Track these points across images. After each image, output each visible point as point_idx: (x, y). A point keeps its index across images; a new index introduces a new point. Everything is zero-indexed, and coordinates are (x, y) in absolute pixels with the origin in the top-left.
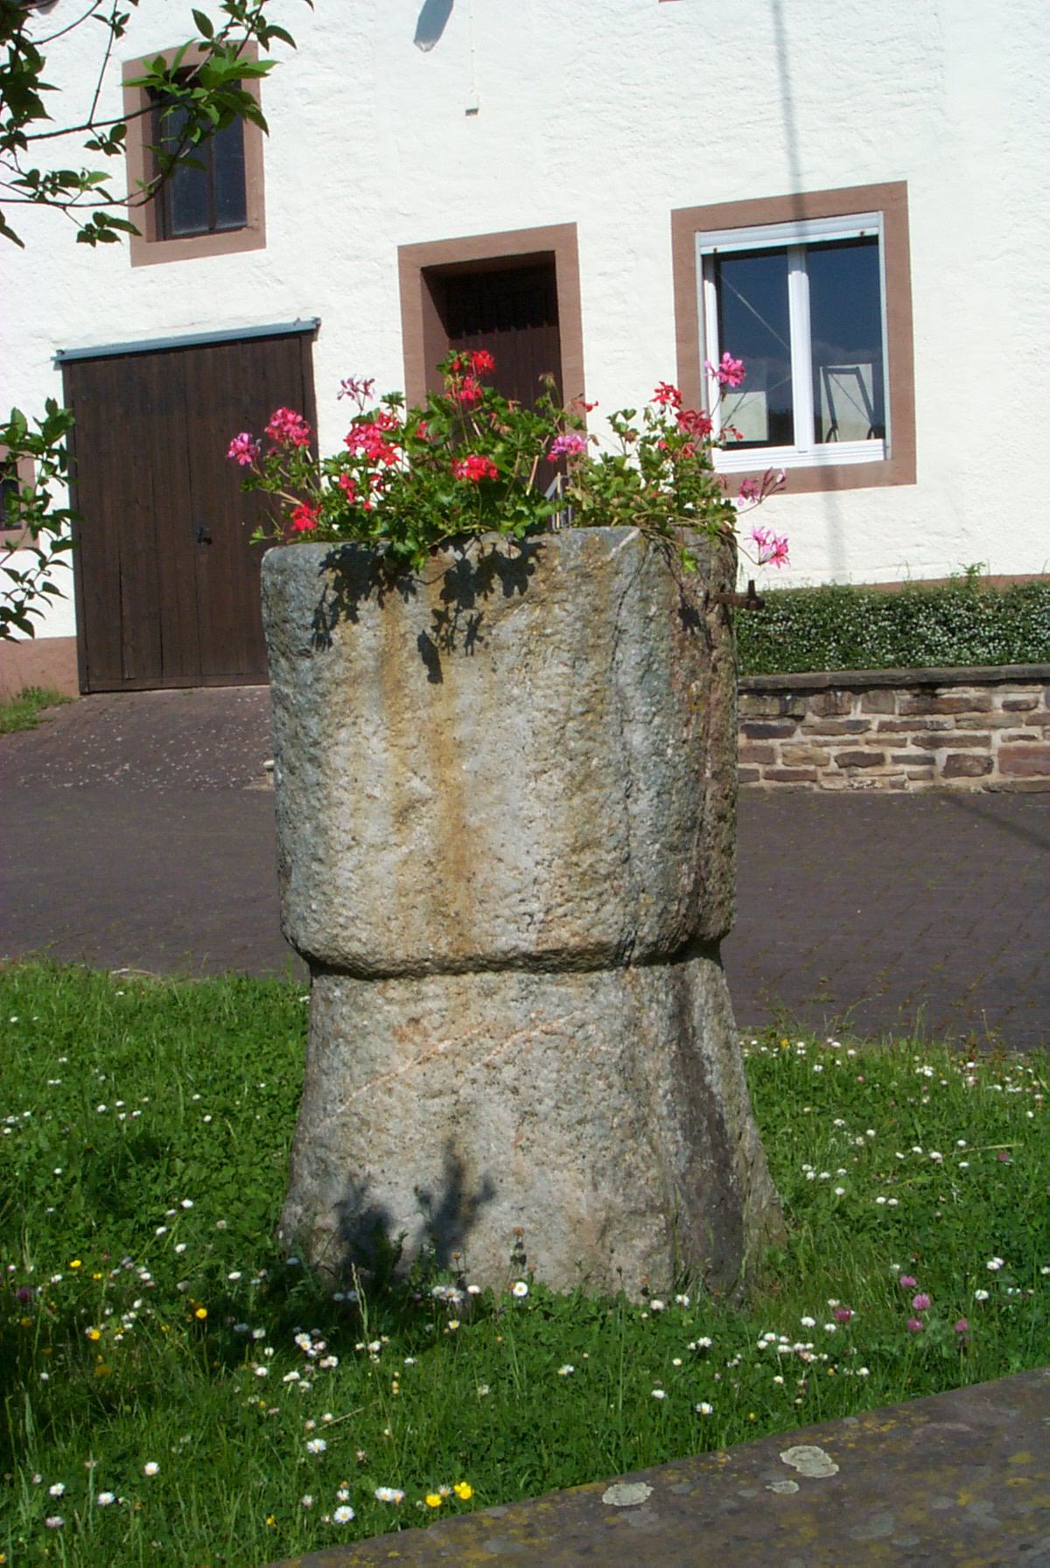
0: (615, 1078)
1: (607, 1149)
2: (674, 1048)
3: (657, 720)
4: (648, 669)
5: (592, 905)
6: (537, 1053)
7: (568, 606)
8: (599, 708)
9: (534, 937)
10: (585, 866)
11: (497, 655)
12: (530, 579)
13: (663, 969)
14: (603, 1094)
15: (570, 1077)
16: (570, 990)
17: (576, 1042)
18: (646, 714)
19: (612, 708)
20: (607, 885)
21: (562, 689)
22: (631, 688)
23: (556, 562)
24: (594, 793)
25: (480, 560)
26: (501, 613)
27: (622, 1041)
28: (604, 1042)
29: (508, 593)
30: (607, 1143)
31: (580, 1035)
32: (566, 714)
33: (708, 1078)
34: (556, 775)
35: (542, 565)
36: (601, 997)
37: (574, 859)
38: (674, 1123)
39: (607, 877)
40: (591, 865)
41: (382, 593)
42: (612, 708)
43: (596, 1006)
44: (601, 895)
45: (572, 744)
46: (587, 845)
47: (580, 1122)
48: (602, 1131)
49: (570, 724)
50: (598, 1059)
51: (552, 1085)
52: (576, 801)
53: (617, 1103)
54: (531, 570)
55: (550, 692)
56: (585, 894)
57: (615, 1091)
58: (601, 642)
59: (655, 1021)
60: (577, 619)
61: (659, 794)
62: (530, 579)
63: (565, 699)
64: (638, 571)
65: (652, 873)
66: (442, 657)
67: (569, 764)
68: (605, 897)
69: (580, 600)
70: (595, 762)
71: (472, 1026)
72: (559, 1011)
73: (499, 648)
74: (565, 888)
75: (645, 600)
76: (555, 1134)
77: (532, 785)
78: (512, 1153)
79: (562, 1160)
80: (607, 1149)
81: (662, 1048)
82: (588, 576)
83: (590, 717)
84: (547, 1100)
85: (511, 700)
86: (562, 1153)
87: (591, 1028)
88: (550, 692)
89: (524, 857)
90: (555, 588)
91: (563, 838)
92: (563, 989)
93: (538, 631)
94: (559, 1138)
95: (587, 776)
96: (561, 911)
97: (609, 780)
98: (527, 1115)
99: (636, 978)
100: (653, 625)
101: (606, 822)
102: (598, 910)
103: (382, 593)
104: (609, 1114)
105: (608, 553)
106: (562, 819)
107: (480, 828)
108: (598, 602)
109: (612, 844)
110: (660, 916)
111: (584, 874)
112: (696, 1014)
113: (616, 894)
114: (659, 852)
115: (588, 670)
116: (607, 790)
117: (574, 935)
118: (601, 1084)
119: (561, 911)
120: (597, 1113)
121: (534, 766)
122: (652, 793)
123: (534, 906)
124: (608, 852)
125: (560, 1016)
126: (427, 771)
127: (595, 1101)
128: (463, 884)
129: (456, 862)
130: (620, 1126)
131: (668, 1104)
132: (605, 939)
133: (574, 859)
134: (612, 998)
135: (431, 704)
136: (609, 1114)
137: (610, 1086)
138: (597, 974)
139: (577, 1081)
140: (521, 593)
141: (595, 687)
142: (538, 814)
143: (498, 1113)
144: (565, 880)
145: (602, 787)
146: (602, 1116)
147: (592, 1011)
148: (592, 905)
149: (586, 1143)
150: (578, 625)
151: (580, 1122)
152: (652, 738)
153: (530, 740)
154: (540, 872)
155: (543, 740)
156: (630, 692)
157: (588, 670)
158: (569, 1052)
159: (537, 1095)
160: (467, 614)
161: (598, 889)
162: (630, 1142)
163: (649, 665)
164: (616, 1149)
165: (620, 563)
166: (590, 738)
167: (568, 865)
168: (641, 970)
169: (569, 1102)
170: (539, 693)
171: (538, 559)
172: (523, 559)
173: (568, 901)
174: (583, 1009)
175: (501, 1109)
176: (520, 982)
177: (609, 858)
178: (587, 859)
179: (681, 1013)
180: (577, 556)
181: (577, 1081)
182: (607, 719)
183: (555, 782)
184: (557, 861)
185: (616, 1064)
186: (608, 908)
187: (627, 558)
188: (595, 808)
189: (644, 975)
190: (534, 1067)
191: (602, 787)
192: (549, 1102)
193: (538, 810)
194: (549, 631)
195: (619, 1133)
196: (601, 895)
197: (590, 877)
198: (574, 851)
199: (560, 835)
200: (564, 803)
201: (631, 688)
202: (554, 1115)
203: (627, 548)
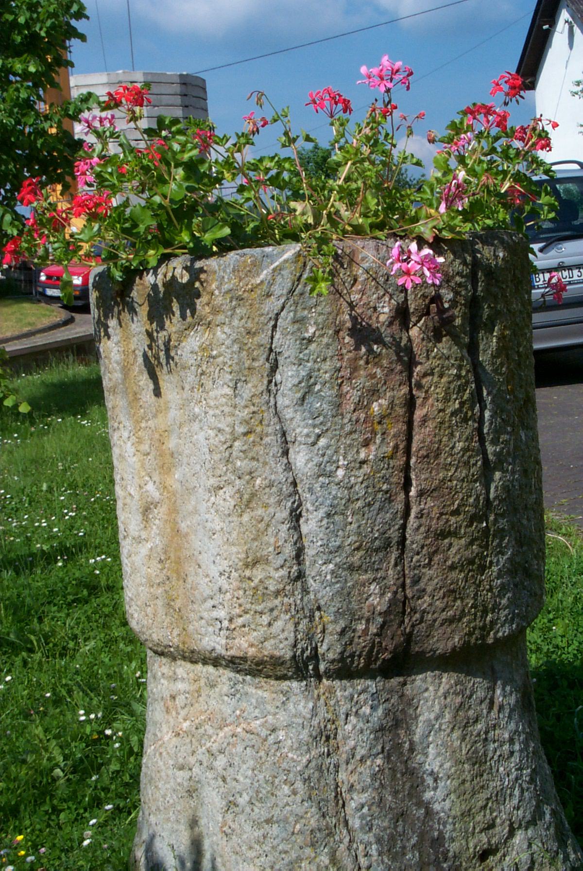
0: (299, 785)
1: (286, 852)
2: (379, 761)
3: (322, 442)
4: (309, 390)
5: (265, 619)
6: (240, 748)
7: (226, 329)
8: (259, 429)
9: (224, 641)
10: (256, 581)
11: (182, 373)
12: (198, 302)
13: (369, 682)
14: (290, 800)
15: (261, 777)
16: (266, 694)
17: (267, 744)
18: (307, 436)
19: (270, 430)
20: (277, 602)
21: (227, 409)
22: (290, 410)
23: (214, 286)
24: (260, 512)
25: (164, 285)
26: (183, 334)
27: (309, 751)
28: (291, 749)
29: (183, 317)
30: (287, 847)
31: (271, 739)
32: (232, 433)
33: (428, 795)
34: (229, 491)
35: (204, 288)
36: (291, 706)
37: (248, 573)
38: (370, 837)
39: (277, 593)
40: (261, 581)
41: (119, 313)
42: (270, 430)
43: (291, 708)
44: (272, 610)
45: (239, 463)
46: (255, 562)
47: (268, 821)
48: (284, 835)
49: (237, 444)
50: (284, 765)
51: (248, 781)
52: (246, 518)
53: (300, 810)
54: (199, 296)
55: (218, 412)
56: (259, 608)
57: (298, 798)
58: (256, 364)
59: (354, 735)
60: (234, 341)
61: (329, 515)
62: (198, 302)
63: (229, 419)
64: (291, 292)
65: (328, 592)
66: (157, 370)
67: (238, 482)
68: (275, 613)
69: (236, 323)
70: (258, 482)
71: (201, 713)
72: (257, 712)
73: (184, 368)
74: (241, 601)
75: (300, 321)
76: (247, 828)
77: (213, 498)
78: (220, 836)
79: (251, 854)
80: (286, 852)
81: (362, 760)
82: (240, 299)
83: (252, 438)
84: (245, 795)
85: (195, 417)
86: (251, 848)
87: (281, 735)
88: (218, 412)
89: (212, 566)
90: (216, 311)
91: (237, 553)
92: (260, 692)
93: (207, 353)
94: (251, 833)
95: (253, 495)
96: (240, 621)
97: (272, 500)
98: (231, 805)
99: (331, 691)
100: (313, 346)
101: (272, 540)
102: (270, 624)
103: (119, 313)
104: (292, 819)
105: (258, 275)
106: (234, 535)
107: (187, 534)
108: (249, 325)
109: (280, 562)
110: (343, 633)
111: (256, 588)
112: (419, 730)
113: (286, 612)
114: (333, 572)
115: (247, 391)
116: (271, 510)
117: (252, 645)
118: (286, 789)
119: (240, 621)
120: (281, 817)
121: (213, 481)
122: (321, 513)
123: (222, 613)
124: (277, 569)
125: (256, 718)
126: (156, 478)
127: (281, 804)
128: (181, 582)
129: (176, 563)
130: (301, 832)
131: (362, 817)
132: (277, 653)
133: (248, 573)
134: (300, 707)
135: (155, 416)
136: (292, 819)
137: (295, 793)
138: (287, 683)
139: (267, 782)
140: (193, 316)
141: (252, 409)
142: (218, 528)
143: (213, 798)
144: (241, 592)
145: (266, 506)
146: (286, 820)
147: (282, 717)
148: (265, 619)
149: (270, 843)
150: (236, 347)
151: (268, 821)
152: (316, 460)
153: (208, 457)
154: (223, 582)
155: (217, 457)
156: (288, 414)
157: (247, 391)
158: (262, 753)
159: (239, 787)
160: (163, 334)
161: (270, 605)
162: (308, 851)
163: (310, 388)
164: (294, 855)
165: (271, 284)
166: (253, 458)
167: (242, 579)
168: (337, 683)
169: (261, 800)
170: (211, 412)
171: (202, 283)
172: (191, 283)
173: (246, 613)
174: (275, 714)
175: (214, 793)
176: (230, 679)
177: (277, 575)
178: (258, 574)
179: (394, 728)
180: (230, 280)
181: (267, 782)
182: (267, 440)
183: (227, 499)
184: (234, 574)
185: (301, 773)
186: (279, 624)
187: (279, 279)
188: (262, 526)
189: (342, 690)
190: (237, 761)
191: (266, 506)
192: (246, 797)
193: (217, 524)
194: (214, 353)
195: (300, 839)
196: (272, 610)
197: (259, 593)
198: (247, 566)
199: (234, 549)
200: (235, 519)
201: (290, 410)
202: (248, 810)
203: (277, 270)
